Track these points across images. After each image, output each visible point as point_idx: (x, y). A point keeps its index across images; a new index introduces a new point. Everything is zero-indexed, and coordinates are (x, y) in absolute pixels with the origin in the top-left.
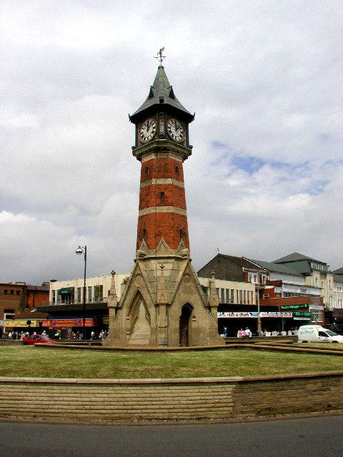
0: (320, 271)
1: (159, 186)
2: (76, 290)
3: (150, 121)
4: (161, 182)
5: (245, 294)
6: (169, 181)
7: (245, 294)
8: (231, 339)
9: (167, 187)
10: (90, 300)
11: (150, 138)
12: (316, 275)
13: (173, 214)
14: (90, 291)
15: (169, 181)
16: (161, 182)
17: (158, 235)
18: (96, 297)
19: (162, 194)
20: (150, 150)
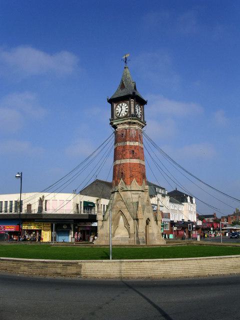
0: (161, 194)
1: (131, 146)
2: (4, 204)
3: (123, 104)
4: (132, 144)
5: (104, 207)
6: (137, 144)
7: (104, 207)
8: (82, 245)
9: (135, 147)
10: (11, 211)
11: (123, 115)
12: (159, 196)
13: (140, 164)
14: (11, 205)
15: (137, 144)
16: (132, 144)
17: (131, 177)
18: (28, 210)
19: (133, 151)
20: (125, 123)
